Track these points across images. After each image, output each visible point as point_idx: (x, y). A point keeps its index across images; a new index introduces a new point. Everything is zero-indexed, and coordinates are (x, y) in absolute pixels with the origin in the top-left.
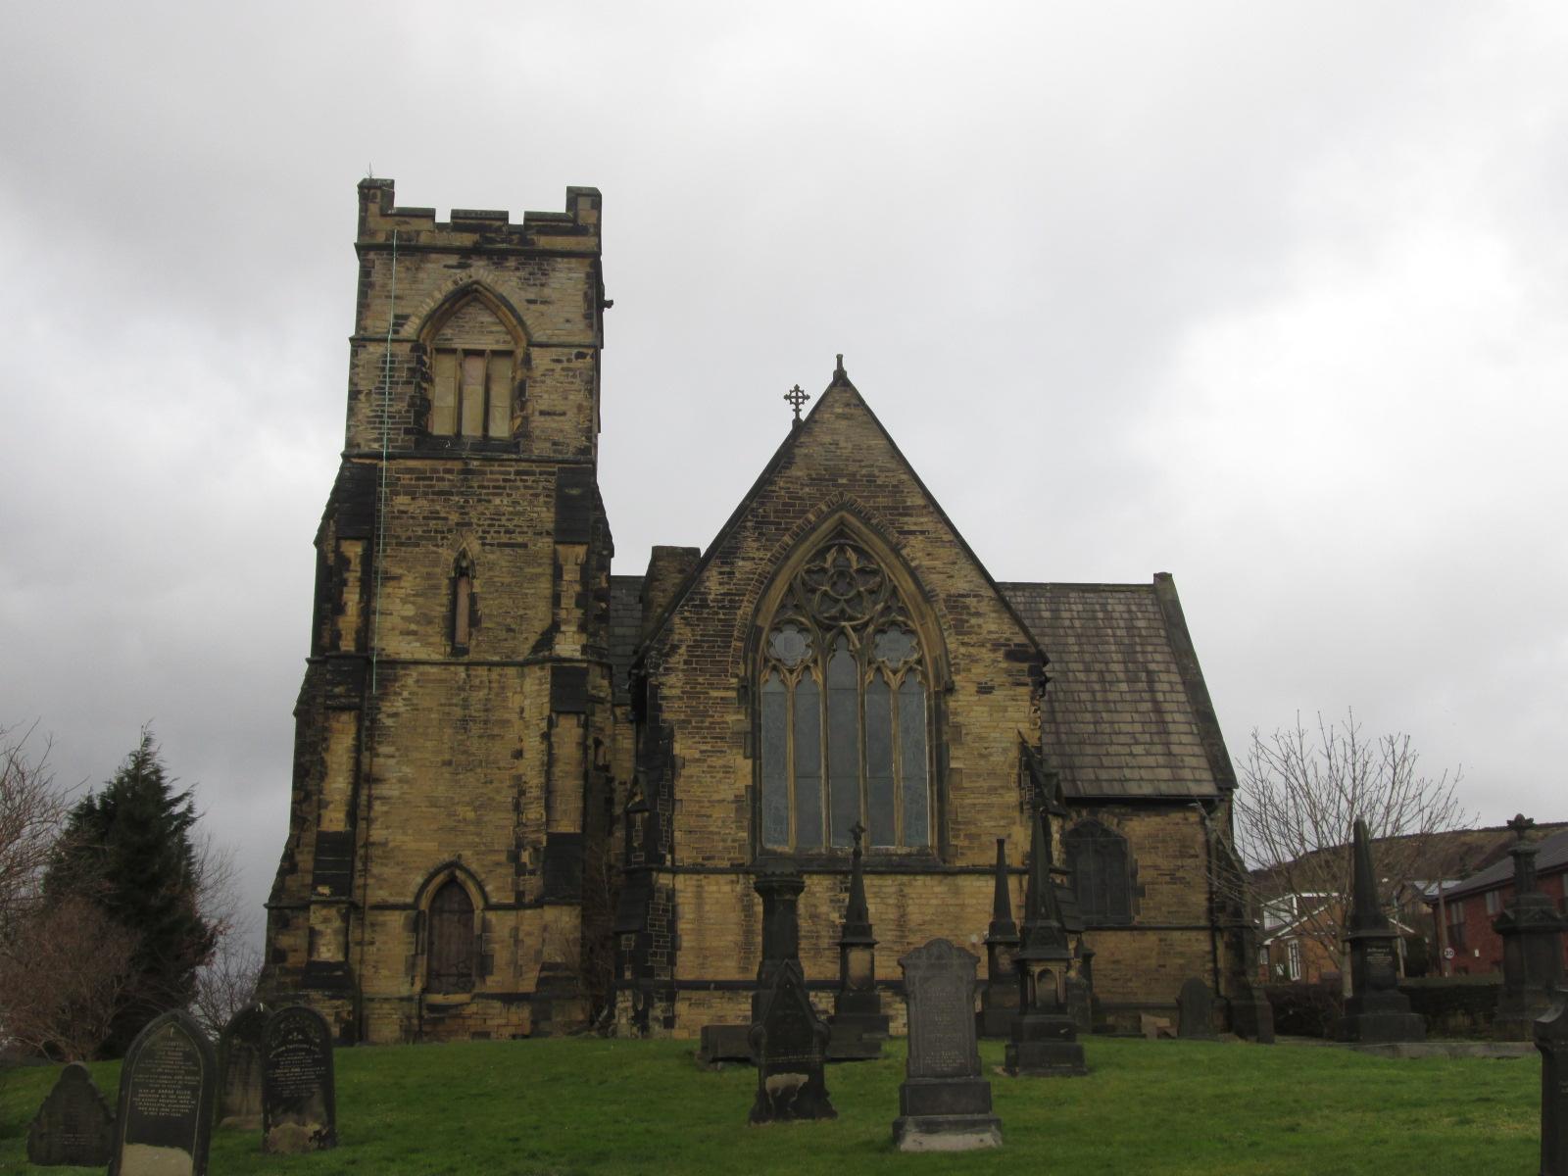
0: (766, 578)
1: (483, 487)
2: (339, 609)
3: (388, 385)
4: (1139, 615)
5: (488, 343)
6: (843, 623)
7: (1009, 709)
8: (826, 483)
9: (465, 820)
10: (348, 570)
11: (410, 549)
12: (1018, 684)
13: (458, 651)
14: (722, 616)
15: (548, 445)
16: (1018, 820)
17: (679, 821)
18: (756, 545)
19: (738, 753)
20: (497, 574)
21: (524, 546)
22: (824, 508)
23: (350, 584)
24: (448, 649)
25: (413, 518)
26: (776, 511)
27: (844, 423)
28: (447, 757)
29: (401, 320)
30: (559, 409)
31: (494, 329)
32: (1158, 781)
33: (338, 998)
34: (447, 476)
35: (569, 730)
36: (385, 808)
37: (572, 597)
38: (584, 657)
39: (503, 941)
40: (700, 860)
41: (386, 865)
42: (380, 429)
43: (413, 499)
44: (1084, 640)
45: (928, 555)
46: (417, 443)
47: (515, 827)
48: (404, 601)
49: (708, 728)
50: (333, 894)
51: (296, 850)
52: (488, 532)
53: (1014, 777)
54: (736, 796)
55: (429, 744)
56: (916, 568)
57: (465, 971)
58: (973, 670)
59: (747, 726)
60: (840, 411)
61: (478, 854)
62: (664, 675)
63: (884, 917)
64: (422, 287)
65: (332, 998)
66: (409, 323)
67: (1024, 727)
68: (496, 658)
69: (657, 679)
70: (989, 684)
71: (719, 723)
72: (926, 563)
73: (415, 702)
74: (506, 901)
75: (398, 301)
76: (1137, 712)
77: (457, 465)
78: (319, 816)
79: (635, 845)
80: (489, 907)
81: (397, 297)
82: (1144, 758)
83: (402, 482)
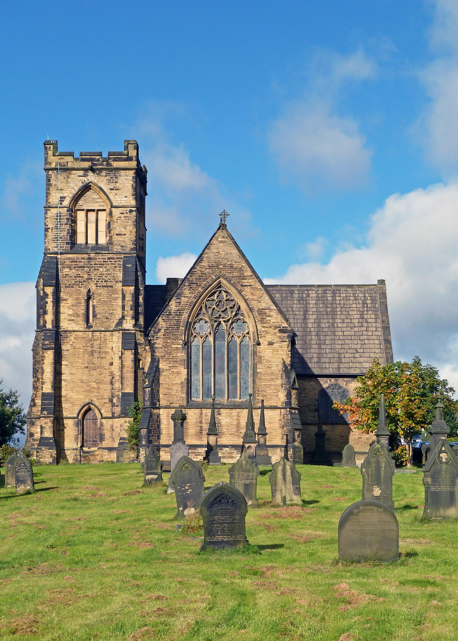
0: (192, 304)
1: (96, 264)
2: (45, 313)
3: (59, 225)
4: (369, 298)
5: (96, 207)
6: (220, 320)
7: (279, 350)
8: (215, 268)
9: (93, 387)
10: (48, 298)
11: (70, 289)
12: (283, 342)
13: (89, 326)
14: (176, 318)
15: (120, 247)
16: (281, 390)
17: (161, 391)
18: (189, 292)
19: (182, 367)
20: (102, 297)
21: (112, 286)
22: (214, 278)
23: (49, 303)
24: (85, 326)
25: (71, 277)
26: (196, 279)
27: (222, 244)
28: (86, 365)
29: (62, 199)
30: (123, 233)
31: (98, 200)
32: (363, 368)
33: (52, 449)
34: (82, 260)
35: (129, 356)
36: (66, 384)
37: (129, 306)
38: (134, 329)
39: (108, 430)
40: (169, 404)
41: (67, 404)
42: (57, 243)
43: (70, 269)
44: (344, 309)
45: (252, 294)
46: (71, 248)
47: (111, 390)
48: (69, 308)
49: (172, 358)
50: (48, 414)
51: (35, 398)
52: (99, 282)
53: (280, 375)
54: (181, 382)
55: (80, 360)
56: (247, 299)
57: (95, 440)
58: (267, 337)
59: (185, 358)
60: (220, 240)
61: (98, 399)
62: (156, 340)
63: (232, 423)
64: (70, 185)
65: (49, 449)
66: (66, 200)
67: (285, 357)
68: (103, 329)
69: (153, 341)
70: (273, 342)
71: (175, 357)
72: (251, 297)
73: (74, 345)
74: (109, 416)
75: (61, 191)
76: (360, 340)
77: (86, 256)
78: (42, 387)
79: (146, 399)
80: (102, 418)
81: (60, 190)
82: (359, 358)
83: (66, 263)
